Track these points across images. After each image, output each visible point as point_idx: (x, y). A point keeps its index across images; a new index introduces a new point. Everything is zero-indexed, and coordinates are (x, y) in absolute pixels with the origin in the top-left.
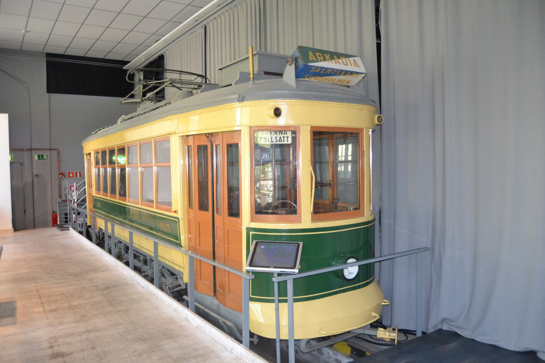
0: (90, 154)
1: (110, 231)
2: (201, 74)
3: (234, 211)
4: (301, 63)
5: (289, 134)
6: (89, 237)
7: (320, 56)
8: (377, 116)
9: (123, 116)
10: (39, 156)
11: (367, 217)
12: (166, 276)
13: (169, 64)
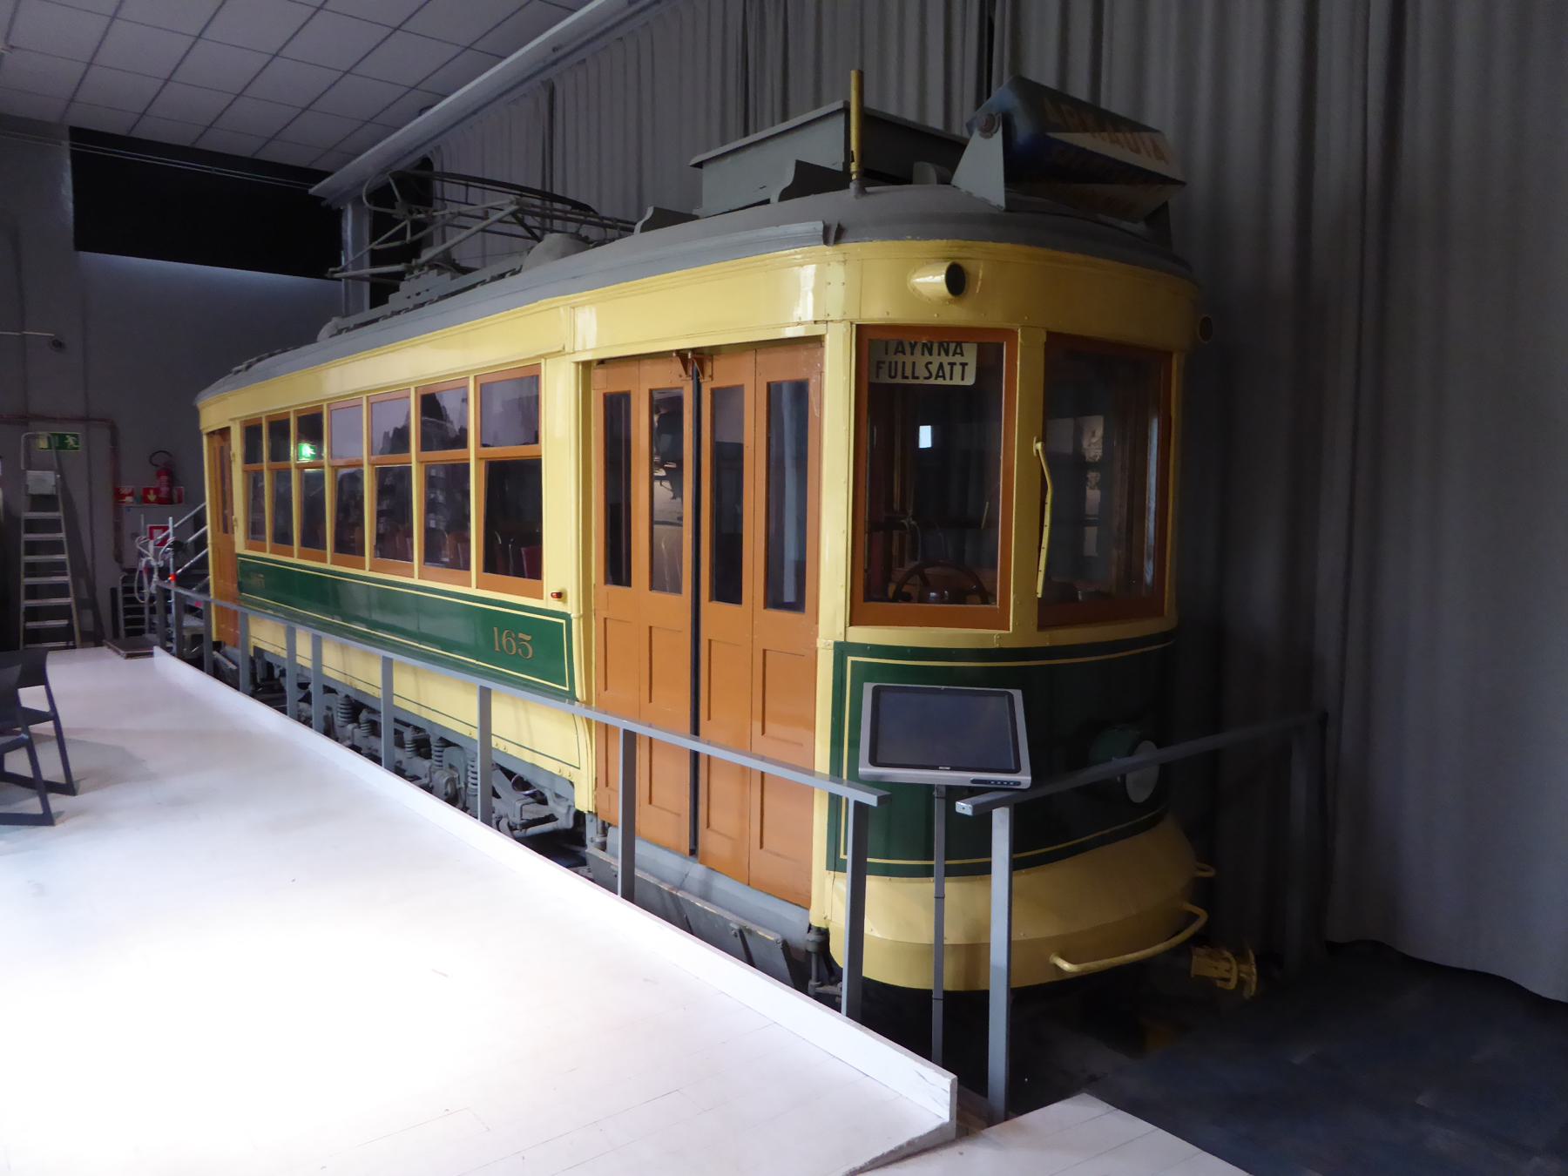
0: (224, 433)
3: (789, 591)
5: (970, 356)
9: (335, 320)
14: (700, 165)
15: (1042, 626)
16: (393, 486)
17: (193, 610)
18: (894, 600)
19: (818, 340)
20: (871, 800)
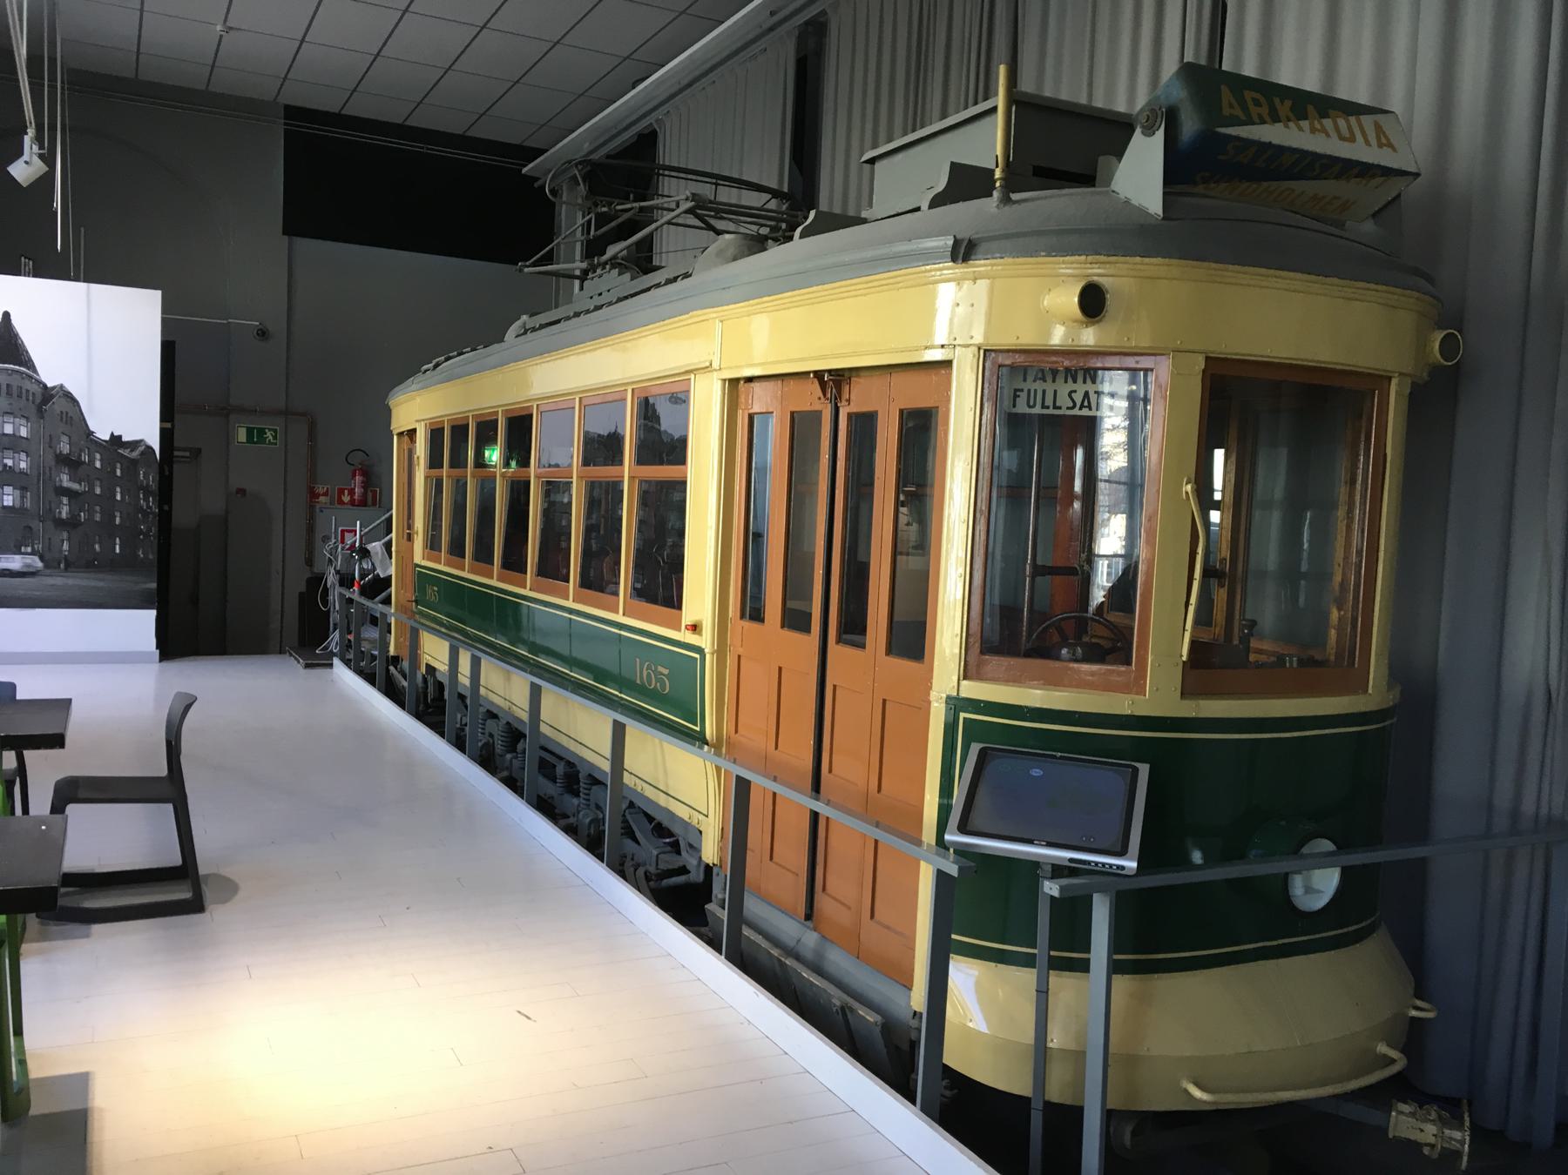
0: (412, 433)
1: (464, 679)
2: (774, 185)
3: (911, 639)
4: (1190, 126)
6: (392, 692)
7: (1257, 103)
8: (1439, 336)
9: (524, 317)
10: (250, 432)
11: (1375, 693)
12: (638, 835)
13: (670, 152)
14: (872, 161)
15: (1185, 693)
16: (603, 499)
17: (374, 621)
18: (1028, 655)
19: (947, 364)
20: (953, 870)
